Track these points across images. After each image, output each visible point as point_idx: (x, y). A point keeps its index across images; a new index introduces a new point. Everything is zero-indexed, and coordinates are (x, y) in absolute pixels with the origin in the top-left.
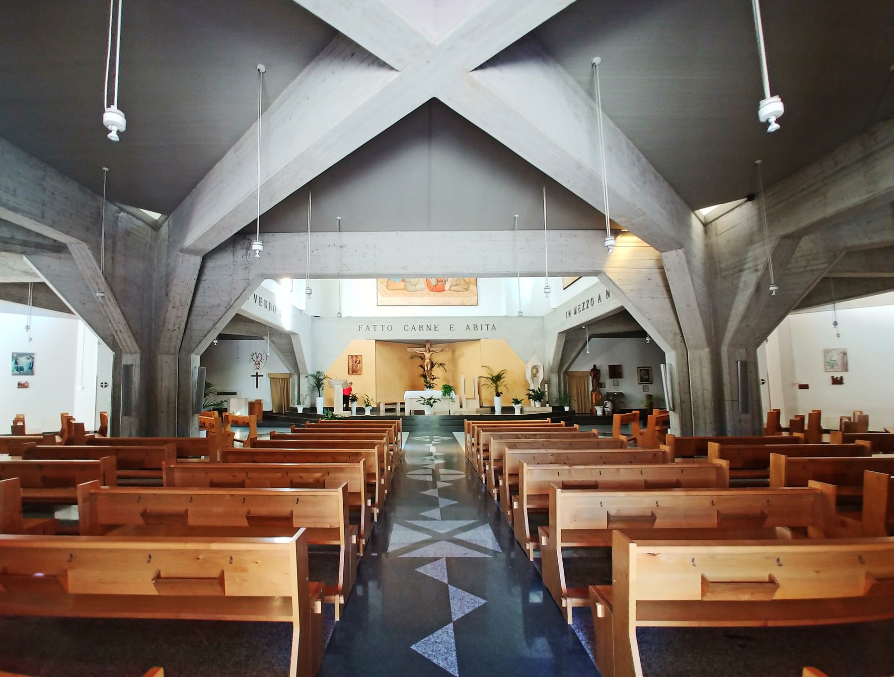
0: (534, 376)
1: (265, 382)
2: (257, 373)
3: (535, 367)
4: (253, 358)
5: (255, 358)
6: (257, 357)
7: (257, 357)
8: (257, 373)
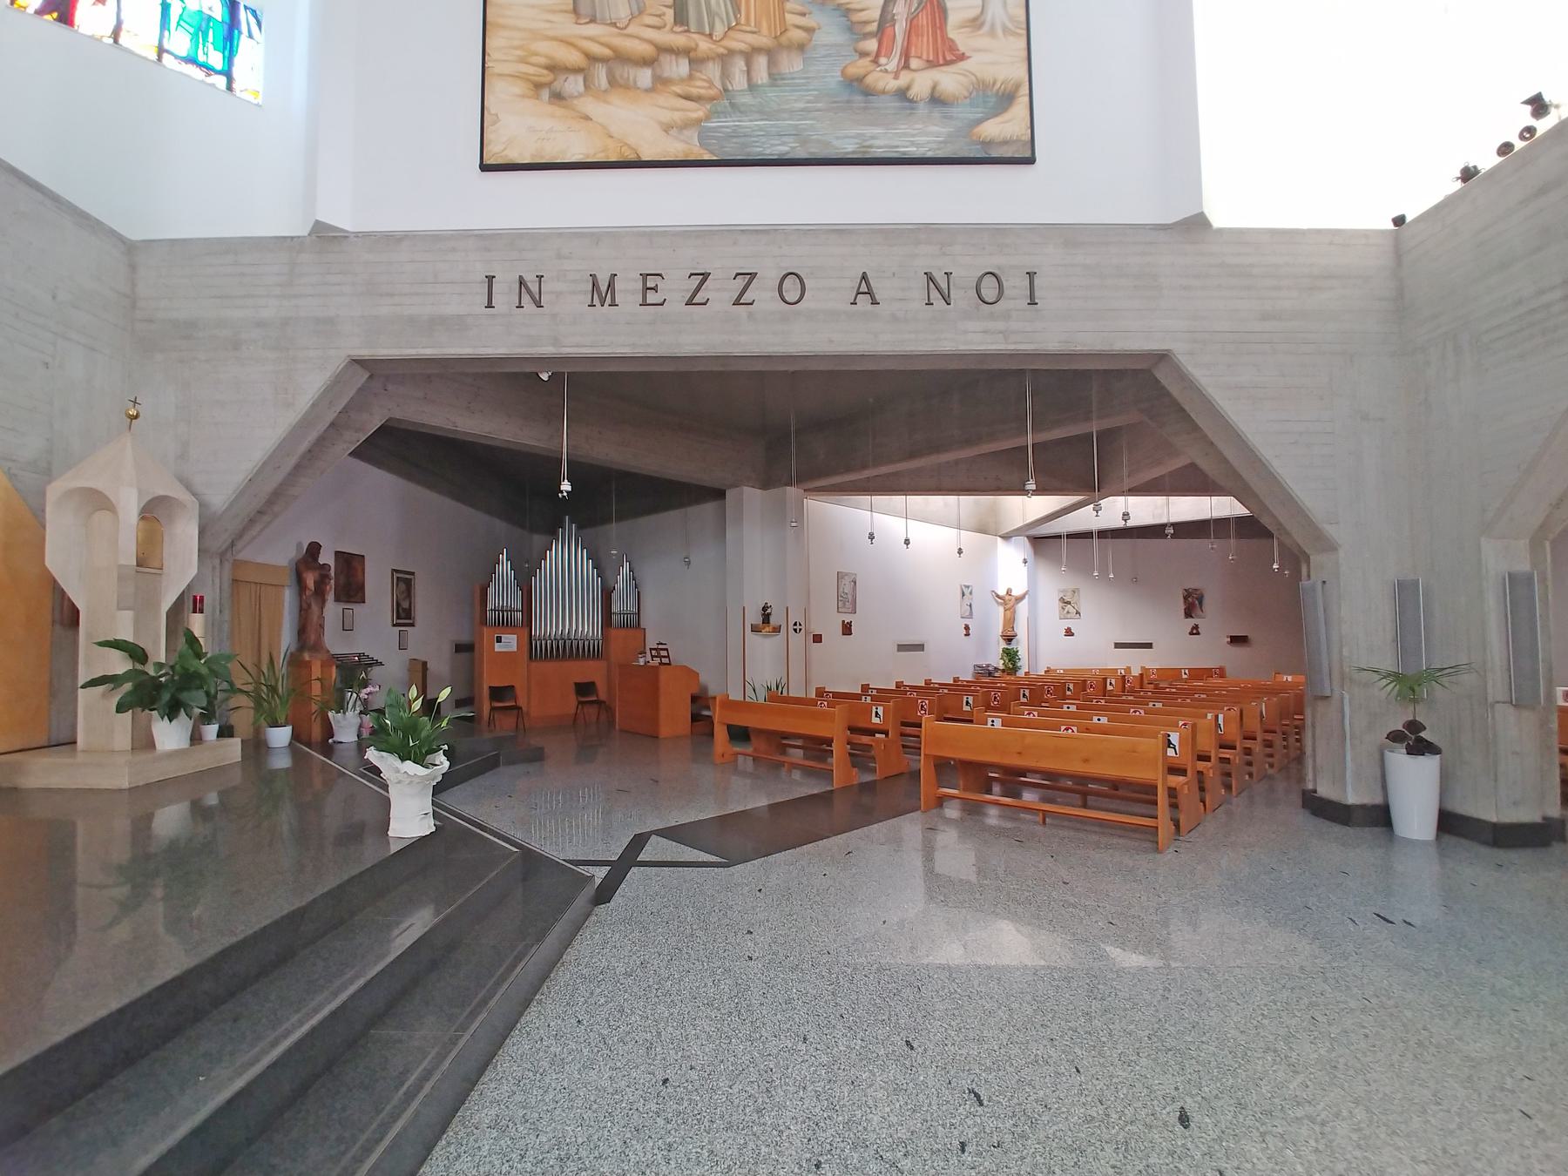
0: (148, 559)
3: (154, 513)
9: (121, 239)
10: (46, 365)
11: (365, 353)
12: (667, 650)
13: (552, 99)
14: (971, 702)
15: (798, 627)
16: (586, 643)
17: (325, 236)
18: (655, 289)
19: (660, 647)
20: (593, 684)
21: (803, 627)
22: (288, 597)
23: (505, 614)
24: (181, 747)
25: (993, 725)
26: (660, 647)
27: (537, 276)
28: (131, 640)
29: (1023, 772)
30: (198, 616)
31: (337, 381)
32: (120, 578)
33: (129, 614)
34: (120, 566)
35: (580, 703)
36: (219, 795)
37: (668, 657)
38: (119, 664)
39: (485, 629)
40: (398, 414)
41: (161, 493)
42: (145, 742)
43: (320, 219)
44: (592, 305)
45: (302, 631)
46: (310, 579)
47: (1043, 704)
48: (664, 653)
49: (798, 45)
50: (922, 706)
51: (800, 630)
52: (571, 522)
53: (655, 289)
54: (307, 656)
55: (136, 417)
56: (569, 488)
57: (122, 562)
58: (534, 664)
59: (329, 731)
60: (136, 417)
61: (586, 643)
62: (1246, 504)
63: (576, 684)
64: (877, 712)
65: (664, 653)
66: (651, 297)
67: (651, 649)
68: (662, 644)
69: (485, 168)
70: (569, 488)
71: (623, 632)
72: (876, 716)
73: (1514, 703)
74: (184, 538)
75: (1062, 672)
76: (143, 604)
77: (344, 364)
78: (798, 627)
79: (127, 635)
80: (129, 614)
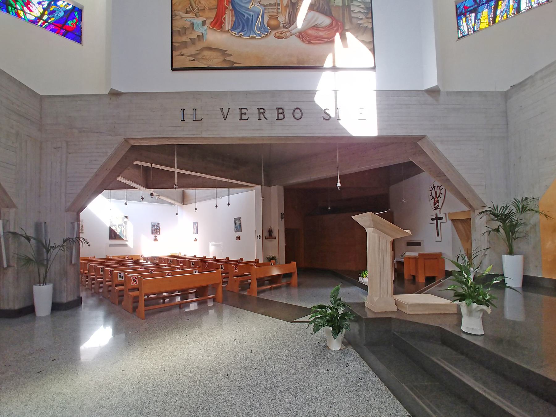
1: (447, 227)
2: (436, 215)
4: (432, 195)
5: (434, 195)
6: (436, 192)
7: (436, 192)
8: (436, 215)
9: (34, 94)
14: (194, 264)
15: (259, 237)
18: (245, 114)
21: (257, 237)
24: (194, 295)
25: (195, 273)
27: (228, 109)
29: (173, 292)
43: (113, 88)
44: (260, 119)
47: (171, 266)
49: (251, 29)
50: (206, 265)
51: (258, 236)
53: (245, 114)
56: (340, 185)
62: (204, 187)
64: (221, 267)
66: (244, 117)
69: (173, 69)
70: (340, 185)
72: (120, 277)
73: (73, 262)
75: (111, 257)
78: (259, 237)
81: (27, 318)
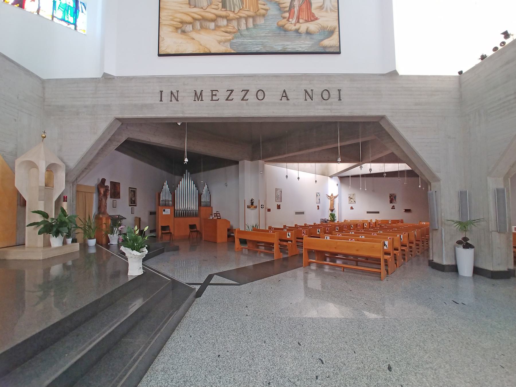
0: (49, 184)
3: (51, 169)
9: (40, 79)
10: (15, 120)
11: (120, 116)
12: (219, 214)
13: (182, 33)
14: (319, 231)
15: (263, 206)
16: (193, 212)
17: (107, 78)
18: (215, 95)
19: (217, 213)
20: (195, 225)
21: (264, 206)
22: (95, 196)
23: (166, 202)
25: (327, 239)
26: (217, 213)
27: (177, 91)
28: (43, 211)
29: (337, 254)
30: (65, 203)
31: (111, 126)
32: (40, 190)
33: (42, 202)
34: (40, 186)
35: (191, 231)
36: (72, 262)
37: (220, 216)
38: (39, 219)
39: (160, 207)
40: (131, 136)
41: (53, 162)
42: (48, 244)
43: (105, 72)
44: (195, 100)
45: (99, 208)
46: (102, 191)
47: (343, 232)
48: (218, 215)
49: (263, 15)
50: (303, 232)
51: (263, 207)
52: (188, 172)
53: (215, 95)
54: (101, 216)
55: (45, 137)
56: (187, 161)
57: (40, 185)
58: (176, 219)
59: (108, 241)
60: (45, 137)
61: (193, 212)
62: (410, 166)
63: (189, 225)
64: (288, 234)
65: (218, 215)
66: (214, 98)
67: (214, 214)
68: (218, 212)
69: (160, 55)
70: (187, 161)
71: (205, 208)
72: (288, 236)
73: (498, 231)
74: (60, 177)
75: (349, 221)
76: (47, 199)
77: (113, 120)
78: (263, 206)
79: (42, 209)
80: (42, 202)
81: (24, 245)
